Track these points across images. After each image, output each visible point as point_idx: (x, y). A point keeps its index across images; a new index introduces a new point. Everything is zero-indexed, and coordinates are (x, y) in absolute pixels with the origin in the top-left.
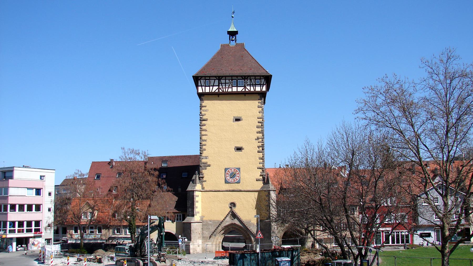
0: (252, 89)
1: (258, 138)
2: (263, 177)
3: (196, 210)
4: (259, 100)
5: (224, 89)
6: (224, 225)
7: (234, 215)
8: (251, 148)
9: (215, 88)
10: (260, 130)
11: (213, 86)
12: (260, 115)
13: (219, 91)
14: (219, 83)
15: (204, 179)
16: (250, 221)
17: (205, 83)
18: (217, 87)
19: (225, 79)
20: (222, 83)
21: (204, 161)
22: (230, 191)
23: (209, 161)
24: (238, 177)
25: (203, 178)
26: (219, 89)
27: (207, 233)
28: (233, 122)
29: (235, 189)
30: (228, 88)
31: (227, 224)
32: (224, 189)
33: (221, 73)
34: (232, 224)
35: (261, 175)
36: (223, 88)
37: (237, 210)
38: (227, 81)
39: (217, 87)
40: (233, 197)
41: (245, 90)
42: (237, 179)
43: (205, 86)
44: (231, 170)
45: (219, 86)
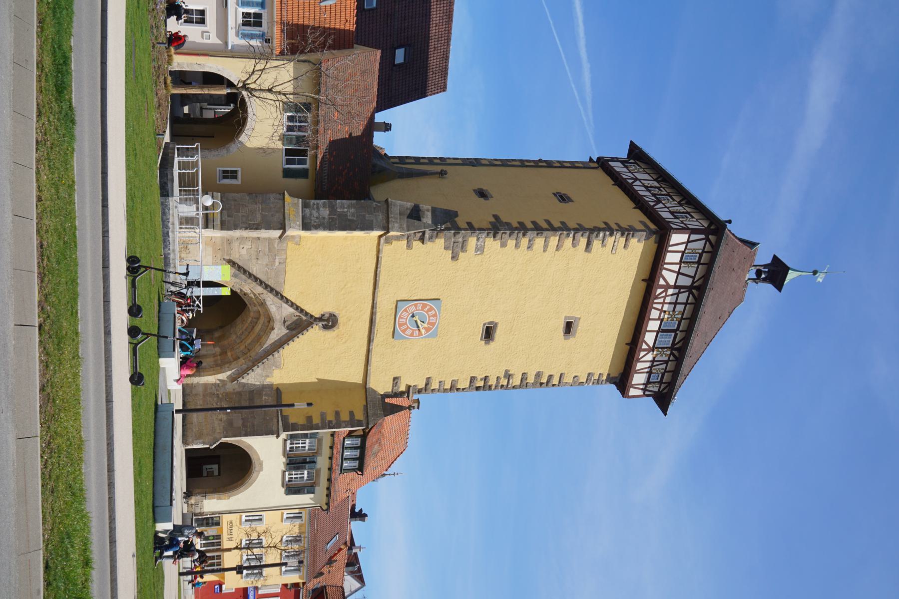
0: (639, 366)
1: (508, 376)
4: (609, 375)
5: (661, 300)
6: (271, 301)
7: (300, 324)
8: (489, 362)
9: (671, 278)
10: (531, 379)
11: (679, 273)
12: (568, 379)
13: (661, 287)
14: (680, 287)
15: (416, 244)
16: (278, 367)
17: (693, 251)
18: (672, 283)
19: (686, 304)
20: (678, 294)
21: (472, 241)
23: (468, 256)
24: (412, 335)
25: (422, 239)
26: (667, 287)
27: (244, 252)
28: (566, 318)
30: (661, 311)
31: (273, 309)
32: (379, 300)
34: (270, 319)
35: (409, 387)
36: (663, 303)
37: (315, 332)
38: (680, 308)
39: (672, 283)
41: (645, 350)
42: (404, 331)
44: (435, 316)
45: (675, 287)
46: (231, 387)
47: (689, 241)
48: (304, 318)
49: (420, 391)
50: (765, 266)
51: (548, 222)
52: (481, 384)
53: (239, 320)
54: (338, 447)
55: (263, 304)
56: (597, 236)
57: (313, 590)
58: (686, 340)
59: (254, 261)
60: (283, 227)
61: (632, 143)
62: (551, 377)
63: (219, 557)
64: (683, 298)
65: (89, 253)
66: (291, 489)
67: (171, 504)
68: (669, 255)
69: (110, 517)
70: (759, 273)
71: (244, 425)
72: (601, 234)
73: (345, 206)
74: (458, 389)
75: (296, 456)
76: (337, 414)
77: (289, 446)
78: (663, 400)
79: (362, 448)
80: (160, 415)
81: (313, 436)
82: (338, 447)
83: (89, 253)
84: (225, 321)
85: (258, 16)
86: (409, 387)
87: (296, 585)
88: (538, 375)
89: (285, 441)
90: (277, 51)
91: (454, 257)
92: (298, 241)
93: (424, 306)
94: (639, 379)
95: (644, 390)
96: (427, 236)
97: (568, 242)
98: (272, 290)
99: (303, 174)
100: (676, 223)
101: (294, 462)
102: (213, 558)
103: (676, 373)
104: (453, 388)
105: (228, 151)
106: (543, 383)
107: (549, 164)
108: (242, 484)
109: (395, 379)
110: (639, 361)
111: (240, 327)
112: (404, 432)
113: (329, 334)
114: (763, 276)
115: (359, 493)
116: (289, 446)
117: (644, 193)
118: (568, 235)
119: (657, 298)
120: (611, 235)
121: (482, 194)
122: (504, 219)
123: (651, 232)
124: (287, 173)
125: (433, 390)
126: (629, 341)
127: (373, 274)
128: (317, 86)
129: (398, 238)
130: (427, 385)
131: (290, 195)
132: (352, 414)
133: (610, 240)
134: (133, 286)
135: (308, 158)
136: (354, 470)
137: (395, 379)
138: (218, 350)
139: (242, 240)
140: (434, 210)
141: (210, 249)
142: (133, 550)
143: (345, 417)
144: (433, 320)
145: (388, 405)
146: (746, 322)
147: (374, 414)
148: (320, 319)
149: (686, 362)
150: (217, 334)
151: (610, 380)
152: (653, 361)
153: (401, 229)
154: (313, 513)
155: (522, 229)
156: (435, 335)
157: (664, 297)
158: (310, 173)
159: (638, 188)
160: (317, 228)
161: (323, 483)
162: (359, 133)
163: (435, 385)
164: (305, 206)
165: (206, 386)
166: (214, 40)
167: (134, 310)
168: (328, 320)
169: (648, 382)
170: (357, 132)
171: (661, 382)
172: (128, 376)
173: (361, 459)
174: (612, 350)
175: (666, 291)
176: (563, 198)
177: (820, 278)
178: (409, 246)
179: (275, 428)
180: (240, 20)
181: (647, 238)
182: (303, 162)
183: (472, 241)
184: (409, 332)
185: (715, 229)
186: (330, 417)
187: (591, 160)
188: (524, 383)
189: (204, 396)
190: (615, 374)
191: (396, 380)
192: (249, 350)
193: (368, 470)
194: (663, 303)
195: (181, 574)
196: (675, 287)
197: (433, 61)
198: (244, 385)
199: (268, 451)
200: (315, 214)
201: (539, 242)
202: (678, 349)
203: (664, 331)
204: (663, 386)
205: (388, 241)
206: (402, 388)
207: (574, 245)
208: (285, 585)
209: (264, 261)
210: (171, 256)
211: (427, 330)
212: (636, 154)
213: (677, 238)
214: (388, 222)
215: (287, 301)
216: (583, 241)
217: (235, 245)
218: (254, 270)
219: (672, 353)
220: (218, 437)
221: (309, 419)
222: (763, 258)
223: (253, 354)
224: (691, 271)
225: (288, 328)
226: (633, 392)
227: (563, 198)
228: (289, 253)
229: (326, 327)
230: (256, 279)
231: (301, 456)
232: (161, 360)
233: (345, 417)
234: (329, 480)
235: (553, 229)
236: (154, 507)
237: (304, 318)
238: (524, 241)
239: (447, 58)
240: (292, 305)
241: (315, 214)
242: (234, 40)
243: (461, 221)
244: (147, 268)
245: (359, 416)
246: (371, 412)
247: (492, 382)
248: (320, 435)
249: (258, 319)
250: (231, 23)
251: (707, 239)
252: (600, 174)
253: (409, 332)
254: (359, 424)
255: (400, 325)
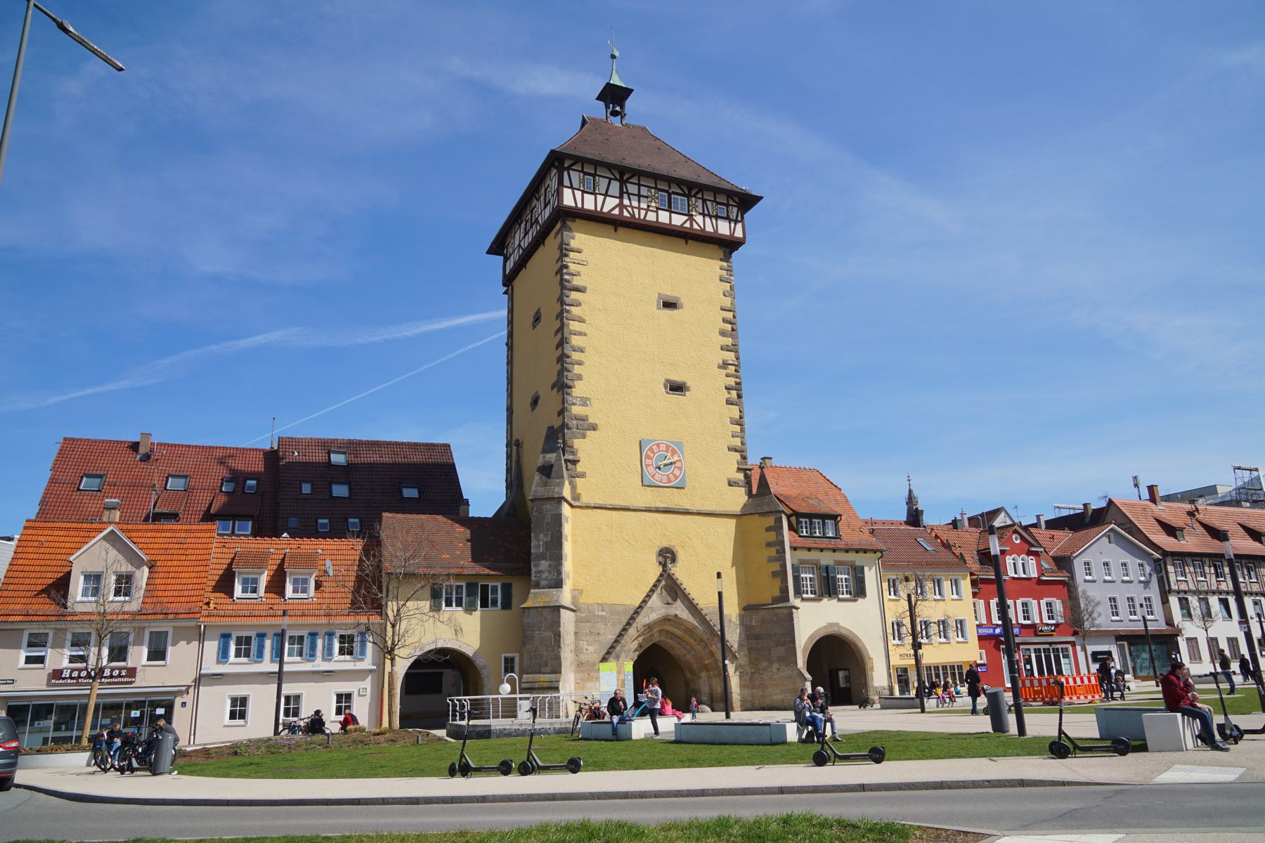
0: (709, 228)
1: (725, 365)
2: (746, 476)
3: (568, 566)
5: (636, 211)
7: (672, 588)
8: (709, 385)
9: (611, 203)
10: (729, 341)
11: (606, 195)
12: (727, 302)
13: (621, 212)
14: (622, 193)
15: (580, 468)
17: (582, 182)
18: (617, 201)
19: (639, 185)
20: (629, 194)
21: (576, 410)
22: (658, 511)
24: (680, 469)
25: (575, 462)
26: (621, 206)
27: (591, 649)
29: (672, 506)
30: (647, 210)
32: (641, 505)
33: (631, 162)
34: (666, 619)
35: (739, 470)
36: (639, 208)
38: (644, 191)
39: (617, 201)
40: (671, 530)
42: (676, 477)
43: (583, 192)
44: (658, 445)
45: (621, 197)
46: (743, 659)
47: (571, 187)
48: (663, 583)
49: (744, 458)
50: (607, 107)
51: (557, 332)
52: (734, 393)
53: (672, 652)
54: (810, 543)
55: (649, 627)
56: (568, 281)
57: (982, 563)
58: (679, 182)
59: (601, 638)
60: (557, 609)
61: (488, 252)
62: (724, 321)
63: (929, 668)
64: (632, 189)
65: (382, 820)
66: (859, 591)
67: (768, 725)
68: (586, 207)
69: (812, 792)
70: (614, 114)
71: (784, 644)
72: (567, 277)
73: (538, 544)
74: (741, 417)
75: (820, 588)
76: (769, 545)
77: (810, 596)
78: (746, 202)
79: (811, 516)
80: (684, 738)
81: (795, 569)
82: (810, 543)
83: (382, 820)
84: (667, 667)
85: (239, 641)
86: (739, 470)
87: (974, 583)
88: (723, 333)
89: (803, 599)
90: (375, 619)
91: (594, 428)
92: (577, 593)
93: (648, 457)
94: (724, 228)
95: (736, 222)
96: (571, 457)
97: (575, 311)
98: (633, 618)
99: (507, 589)
100: (554, 202)
101: (828, 588)
102: (929, 676)
103: (716, 191)
104: (739, 422)
105: (484, 667)
106: (732, 328)
107: (510, 335)
108: (855, 645)
109: (730, 485)
110: (703, 230)
111: (678, 651)
112: (797, 472)
113: (681, 555)
114: (618, 109)
115: (862, 517)
116: (810, 596)
117: (530, 236)
118: (568, 311)
119: (633, 216)
120: (567, 267)
121: (535, 402)
122: (555, 378)
123: (564, 226)
124: (507, 605)
125: (742, 444)
126: (683, 241)
127: (614, 512)
128: (410, 576)
129: (573, 487)
130: (736, 451)
131: (525, 601)
132: (768, 529)
133: (573, 267)
134: (479, 770)
135: (490, 584)
136: (836, 524)
137: (730, 485)
138: (703, 674)
139: (577, 650)
140: (545, 451)
141: (589, 684)
142: (984, 761)
143: (772, 536)
144: (663, 447)
145: (759, 490)
146: (683, 122)
147: (768, 505)
148: (664, 566)
149: (704, 180)
150: (689, 675)
151: (727, 258)
152: (704, 215)
153: (561, 485)
154: (887, 566)
155: (562, 359)
156: (680, 445)
157: (633, 208)
158: (507, 581)
159: (525, 244)
160: (560, 573)
161: (851, 557)
162: (468, 531)
163: (737, 442)
164: (537, 586)
165: (742, 686)
166: (367, 684)
167: (505, 769)
168: (666, 558)
169: (728, 218)
170: (467, 533)
171: (727, 205)
172: (875, 766)
173: (824, 517)
174: (734, 530)
175: (626, 207)
176: (537, 319)
177: (617, 54)
178: (583, 475)
179: (786, 611)
180: (348, 657)
181: (570, 230)
182: (495, 589)
183: (576, 410)
184: (677, 472)
185: (557, 162)
186: (773, 552)
187: (505, 293)
188: (733, 348)
189: (754, 687)
190: (721, 254)
191: (731, 484)
192: (702, 641)
193: (837, 510)
194: (639, 208)
195: (923, 711)
196: (621, 197)
197: (418, 458)
198: (740, 645)
199: (812, 619)
200: (546, 575)
201: (575, 341)
202: (690, 190)
203: (670, 206)
204: (731, 202)
205: (576, 497)
206: (741, 476)
207: (579, 304)
208: (975, 595)
209: (601, 627)
210: (557, 726)
211: (674, 452)
212: (498, 247)
213: (568, 199)
214: (553, 499)
215: (645, 602)
216: (574, 295)
217: (583, 657)
218: (611, 637)
219: (695, 196)
220: (796, 672)
221: (775, 574)
222: (599, 110)
223: (705, 637)
224: (603, 183)
225: (675, 600)
226: (739, 233)
227: (537, 319)
228: (591, 601)
229: (674, 560)
230: (620, 635)
231: (820, 583)
232: (634, 737)
233: (772, 536)
234: (847, 551)
235: (561, 329)
236: (772, 744)
237: (663, 583)
238: (575, 356)
239: (416, 444)
240: (649, 596)
241: (546, 575)
242: (367, 663)
243: (557, 425)
244: (462, 756)
245: (770, 521)
246: (766, 509)
247: (731, 381)
248: (796, 562)
249: (668, 632)
250: (308, 667)
251: (569, 168)
252: (518, 283)
253: (677, 472)
254: (779, 521)
255: (670, 481)
